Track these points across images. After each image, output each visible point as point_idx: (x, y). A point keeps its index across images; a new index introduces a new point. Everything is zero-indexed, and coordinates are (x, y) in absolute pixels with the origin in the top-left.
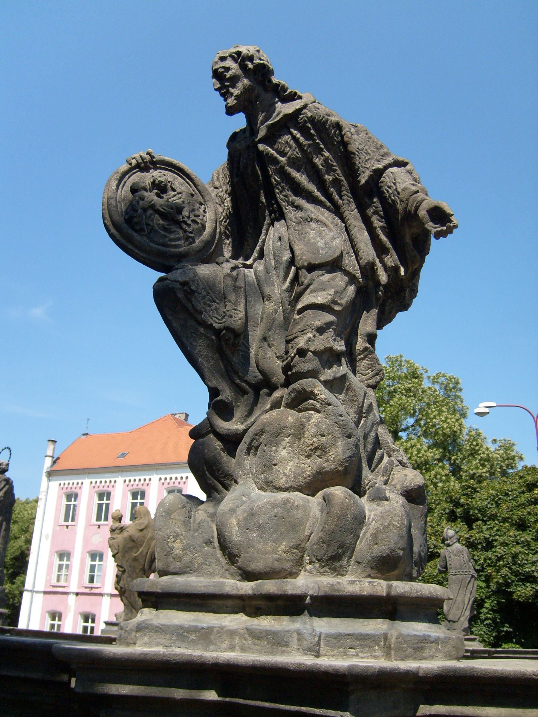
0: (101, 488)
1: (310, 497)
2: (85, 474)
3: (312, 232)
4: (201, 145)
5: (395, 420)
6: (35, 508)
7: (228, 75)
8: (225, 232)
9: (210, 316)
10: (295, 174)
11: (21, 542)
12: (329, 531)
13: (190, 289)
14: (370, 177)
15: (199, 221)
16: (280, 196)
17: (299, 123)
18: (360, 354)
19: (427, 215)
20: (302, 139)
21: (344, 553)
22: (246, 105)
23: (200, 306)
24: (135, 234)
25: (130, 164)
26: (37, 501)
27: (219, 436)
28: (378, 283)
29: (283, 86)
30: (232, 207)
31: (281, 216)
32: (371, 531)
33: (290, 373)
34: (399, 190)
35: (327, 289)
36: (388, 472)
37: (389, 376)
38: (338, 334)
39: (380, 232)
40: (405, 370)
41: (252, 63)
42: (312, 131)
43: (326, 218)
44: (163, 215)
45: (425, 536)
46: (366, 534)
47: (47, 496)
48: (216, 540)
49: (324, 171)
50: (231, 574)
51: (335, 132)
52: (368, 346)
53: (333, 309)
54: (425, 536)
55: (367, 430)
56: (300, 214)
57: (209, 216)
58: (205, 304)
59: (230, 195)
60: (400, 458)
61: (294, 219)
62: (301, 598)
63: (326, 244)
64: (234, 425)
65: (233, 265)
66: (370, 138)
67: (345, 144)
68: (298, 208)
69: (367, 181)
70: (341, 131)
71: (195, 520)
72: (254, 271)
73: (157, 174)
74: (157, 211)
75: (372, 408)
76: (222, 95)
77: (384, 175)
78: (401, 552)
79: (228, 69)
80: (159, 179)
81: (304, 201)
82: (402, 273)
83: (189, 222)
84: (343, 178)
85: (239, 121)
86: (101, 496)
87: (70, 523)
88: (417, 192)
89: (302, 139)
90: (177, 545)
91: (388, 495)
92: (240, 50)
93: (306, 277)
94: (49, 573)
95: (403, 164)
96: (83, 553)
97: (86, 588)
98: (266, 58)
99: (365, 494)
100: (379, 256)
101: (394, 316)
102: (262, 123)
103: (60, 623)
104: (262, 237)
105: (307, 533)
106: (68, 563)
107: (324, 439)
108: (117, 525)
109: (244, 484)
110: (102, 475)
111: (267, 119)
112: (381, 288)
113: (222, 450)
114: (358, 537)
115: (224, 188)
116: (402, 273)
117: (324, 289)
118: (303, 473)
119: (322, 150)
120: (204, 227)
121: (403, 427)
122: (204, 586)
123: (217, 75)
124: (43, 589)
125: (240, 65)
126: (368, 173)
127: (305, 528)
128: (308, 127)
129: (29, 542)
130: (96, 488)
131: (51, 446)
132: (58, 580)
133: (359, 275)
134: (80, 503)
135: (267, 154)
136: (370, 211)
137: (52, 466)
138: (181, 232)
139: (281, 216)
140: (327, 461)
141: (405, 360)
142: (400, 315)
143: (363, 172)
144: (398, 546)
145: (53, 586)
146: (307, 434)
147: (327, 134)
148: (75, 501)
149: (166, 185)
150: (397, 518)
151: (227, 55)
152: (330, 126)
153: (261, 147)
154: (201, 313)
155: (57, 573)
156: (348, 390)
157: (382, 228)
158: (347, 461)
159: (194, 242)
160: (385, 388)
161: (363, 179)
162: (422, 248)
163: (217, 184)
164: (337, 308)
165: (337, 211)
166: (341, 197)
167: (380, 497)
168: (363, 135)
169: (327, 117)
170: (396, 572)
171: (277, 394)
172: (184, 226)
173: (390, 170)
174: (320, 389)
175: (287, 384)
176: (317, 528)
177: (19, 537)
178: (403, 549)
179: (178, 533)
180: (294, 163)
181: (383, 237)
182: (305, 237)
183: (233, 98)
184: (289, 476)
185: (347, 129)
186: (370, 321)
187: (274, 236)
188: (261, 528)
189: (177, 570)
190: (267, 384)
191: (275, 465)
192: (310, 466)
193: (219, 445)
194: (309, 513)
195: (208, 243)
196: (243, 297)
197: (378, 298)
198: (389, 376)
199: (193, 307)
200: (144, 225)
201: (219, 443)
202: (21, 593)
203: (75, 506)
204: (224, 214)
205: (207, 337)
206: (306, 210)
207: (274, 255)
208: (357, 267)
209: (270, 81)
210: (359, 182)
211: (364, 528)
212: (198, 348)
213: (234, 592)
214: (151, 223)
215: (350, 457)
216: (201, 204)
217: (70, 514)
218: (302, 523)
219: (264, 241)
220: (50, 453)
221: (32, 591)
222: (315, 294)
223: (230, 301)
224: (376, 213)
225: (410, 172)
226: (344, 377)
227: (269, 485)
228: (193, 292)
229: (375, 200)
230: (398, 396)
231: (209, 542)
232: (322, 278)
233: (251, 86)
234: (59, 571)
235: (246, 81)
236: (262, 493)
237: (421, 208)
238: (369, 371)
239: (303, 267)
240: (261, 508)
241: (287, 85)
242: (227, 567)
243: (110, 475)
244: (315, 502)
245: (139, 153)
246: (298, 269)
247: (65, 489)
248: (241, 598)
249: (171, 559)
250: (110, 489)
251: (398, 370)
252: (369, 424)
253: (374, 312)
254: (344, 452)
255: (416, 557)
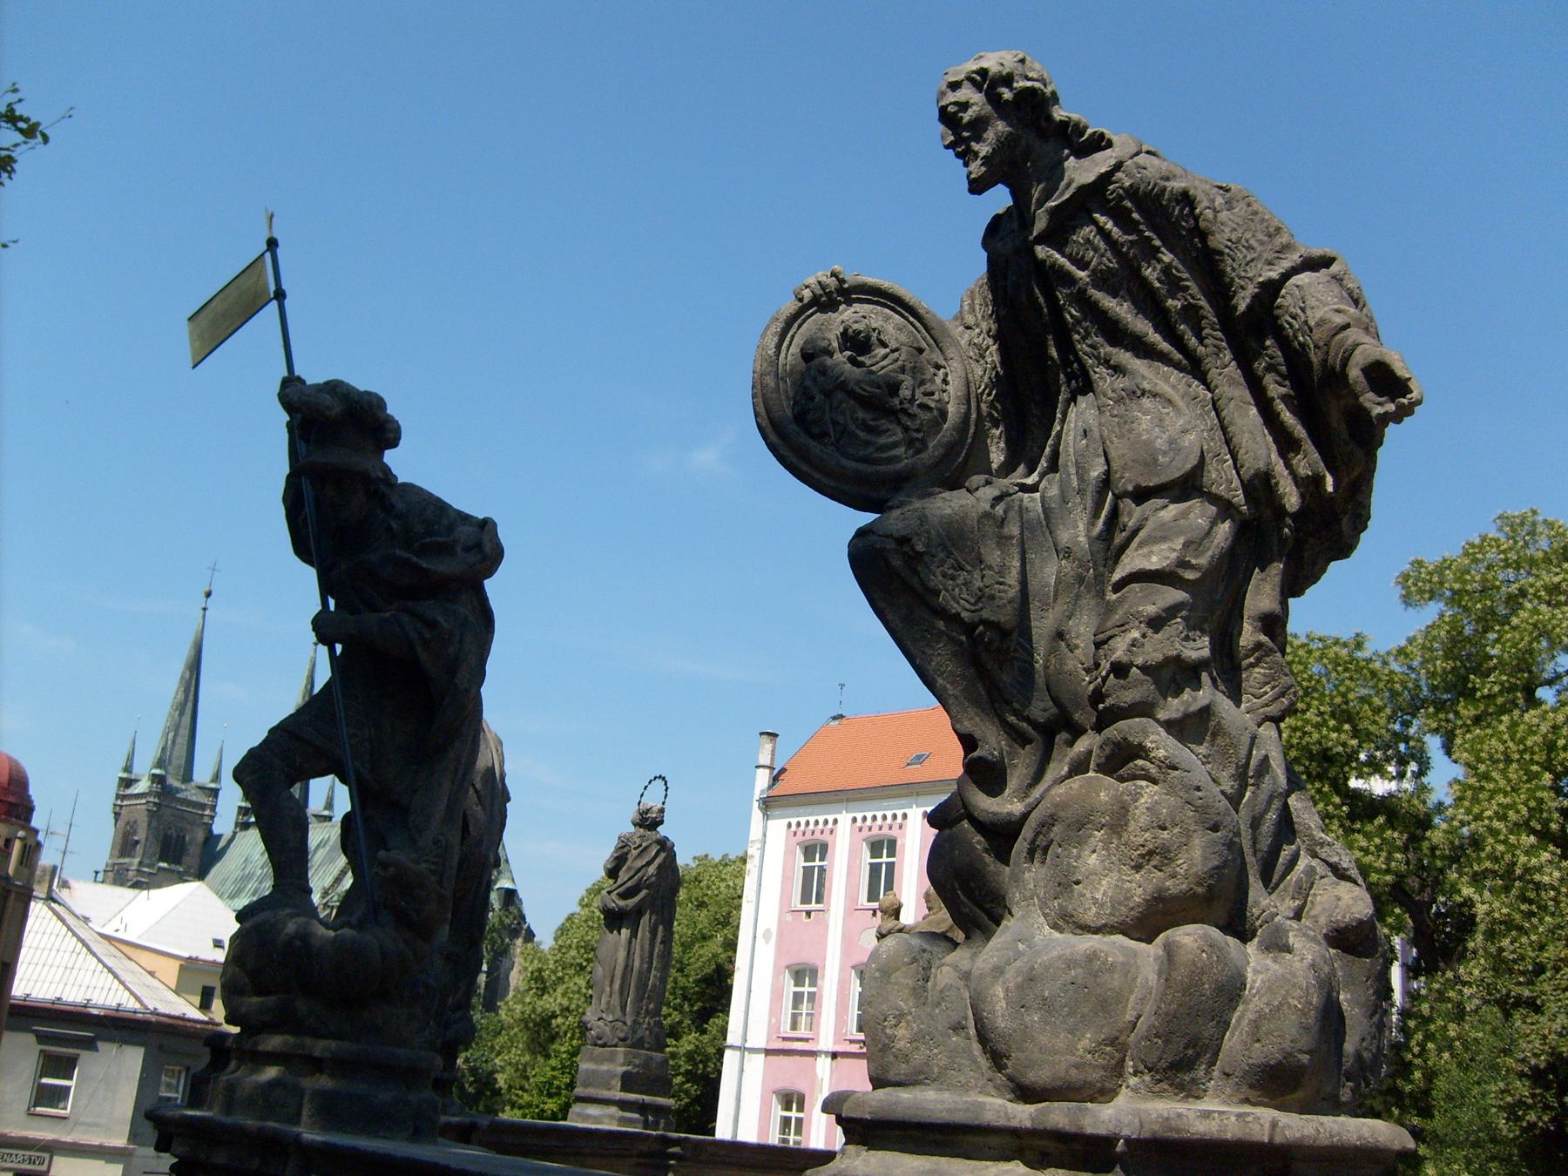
0: (875, 831)
1: (1143, 945)
2: (841, 801)
3: (1144, 418)
4: (933, 251)
5: (1525, 660)
6: (740, 875)
7: (967, 117)
8: (990, 414)
9: (954, 598)
10: (1108, 303)
11: (715, 946)
12: (1167, 1014)
13: (913, 549)
14: (1255, 297)
15: (933, 405)
16: (1082, 347)
17: (1109, 201)
18: (1247, 657)
19: (1362, 379)
20: (1116, 232)
21: (1198, 1056)
22: (1004, 168)
23: (936, 580)
24: (812, 443)
25: (801, 300)
26: (744, 860)
27: (980, 826)
28: (1281, 511)
29: (1077, 124)
30: (1002, 363)
31: (1087, 387)
32: (1250, 1016)
33: (1101, 706)
34: (1312, 323)
35: (1171, 537)
36: (1304, 890)
37: (1506, 560)
38: (1195, 625)
39: (1280, 406)
40: (1544, 543)
41: (1011, 88)
42: (1135, 216)
43: (1173, 387)
44: (866, 402)
45: (1376, 1019)
46: (1242, 1017)
47: (763, 849)
48: (971, 1023)
49: (1163, 292)
50: (997, 1088)
51: (1181, 210)
52: (1263, 638)
53: (1181, 579)
54: (1376, 1019)
55: (1258, 810)
56: (1122, 383)
57: (954, 389)
58: (944, 575)
59: (996, 338)
60: (1335, 859)
61: (1111, 394)
62: (1108, 1141)
63: (1171, 442)
64: (1007, 805)
65: (997, 493)
66: (1256, 213)
67: (1204, 235)
68: (1118, 370)
69: (1248, 307)
70: (1193, 208)
71: (935, 985)
72: (1039, 492)
73: (848, 315)
74: (851, 394)
75: (1269, 766)
76: (958, 155)
77: (1283, 291)
78: (1305, 1058)
79: (964, 106)
80: (855, 326)
81: (1128, 355)
82: (1330, 489)
83: (914, 410)
84: (1203, 303)
85: (999, 199)
86: (876, 848)
87: (813, 906)
88: (1347, 326)
89: (1116, 232)
90: (901, 1032)
91: (1291, 941)
92: (985, 65)
93: (1132, 514)
94: (775, 1010)
95: (1325, 262)
96: (842, 970)
97: (852, 1042)
98: (1041, 70)
99: (1254, 935)
100: (1283, 454)
101: (1324, 571)
102: (1040, 204)
103: (800, 1115)
104: (1057, 427)
105: (1129, 1016)
106: (813, 989)
107: (1165, 835)
108: (891, 923)
109: (1023, 917)
110: (876, 803)
111: (1047, 195)
112: (1289, 521)
113: (986, 851)
114: (1228, 1024)
115: (984, 325)
116: (1330, 489)
117: (1164, 539)
118: (1127, 899)
119: (1157, 250)
120: (943, 414)
121: (1546, 675)
122: (948, 1110)
123: (948, 118)
124: (762, 1045)
125: (987, 95)
126: (1252, 289)
127: (1125, 1007)
128: (1126, 208)
129: (731, 945)
130: (865, 830)
131: (768, 746)
132: (794, 1026)
133: (1239, 498)
134: (832, 863)
135: (1054, 264)
136: (1260, 366)
137: (770, 787)
138: (899, 430)
139: (1087, 387)
140: (1173, 876)
141: (1545, 521)
142: (1335, 567)
143: (1242, 288)
144: (1298, 1046)
145: (784, 1039)
146: (1132, 826)
147: (1166, 216)
148: (822, 859)
149: (868, 337)
150: (1298, 993)
151: (962, 77)
152: (1169, 200)
153: (1041, 251)
154: (938, 593)
155: (790, 1011)
156: (1214, 735)
157: (1284, 398)
158: (1212, 876)
159: (925, 446)
160: (1498, 588)
161: (1242, 303)
162: (1367, 435)
163: (970, 320)
164: (1190, 575)
165: (1195, 368)
166: (1201, 340)
167: (1277, 945)
168: (1240, 208)
169: (1162, 183)
170: (1300, 1094)
171: (1081, 745)
172: (904, 419)
173: (1293, 280)
174: (1155, 737)
175: (1099, 728)
176: (1149, 1009)
177: (711, 937)
178: (1309, 1052)
179: (901, 1010)
180: (1105, 281)
181: (1287, 417)
182: (1130, 431)
183: (979, 162)
184: (1102, 905)
185: (1205, 203)
186: (1267, 588)
187: (1079, 421)
188: (1046, 1005)
189: (903, 1078)
190: (1062, 726)
191: (1078, 883)
192: (1139, 887)
193: (979, 842)
194: (1135, 979)
195: (952, 448)
196: (1017, 557)
197: (1283, 541)
198: (1506, 560)
199: (923, 584)
200: (830, 418)
201: (979, 838)
202: (720, 1053)
203: (822, 870)
204: (986, 379)
205: (952, 640)
206: (1133, 373)
207: (1077, 463)
208: (1236, 483)
209: (1049, 118)
210: (1235, 308)
211: (1240, 1008)
212: (936, 660)
213: (1002, 1122)
214: (841, 420)
215: (1217, 868)
216: (938, 367)
217: (813, 887)
218: (1121, 998)
219: (1060, 432)
220: (765, 759)
221: (742, 1049)
222: (1145, 550)
223: (990, 568)
224: (1271, 368)
225: (1337, 279)
226: (1206, 712)
227: (1067, 921)
228: (920, 555)
229: (1268, 343)
230: (1529, 606)
231: (958, 1028)
232: (1162, 513)
233: (1014, 133)
234: (795, 1006)
235: (1001, 126)
236: (1056, 935)
237: (1352, 362)
238: (1267, 688)
239: (1125, 494)
240: (1047, 968)
241: (1084, 120)
242: (990, 1074)
243: (893, 802)
244: (1149, 953)
245: (816, 276)
246: (1117, 497)
247: (799, 834)
248: (1015, 1133)
249: (891, 1058)
250: (895, 833)
251: (1526, 544)
252: (1263, 797)
253: (1277, 567)
254: (1205, 858)
255: (1348, 1062)
